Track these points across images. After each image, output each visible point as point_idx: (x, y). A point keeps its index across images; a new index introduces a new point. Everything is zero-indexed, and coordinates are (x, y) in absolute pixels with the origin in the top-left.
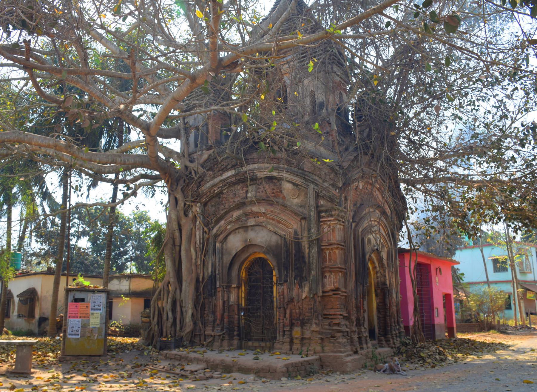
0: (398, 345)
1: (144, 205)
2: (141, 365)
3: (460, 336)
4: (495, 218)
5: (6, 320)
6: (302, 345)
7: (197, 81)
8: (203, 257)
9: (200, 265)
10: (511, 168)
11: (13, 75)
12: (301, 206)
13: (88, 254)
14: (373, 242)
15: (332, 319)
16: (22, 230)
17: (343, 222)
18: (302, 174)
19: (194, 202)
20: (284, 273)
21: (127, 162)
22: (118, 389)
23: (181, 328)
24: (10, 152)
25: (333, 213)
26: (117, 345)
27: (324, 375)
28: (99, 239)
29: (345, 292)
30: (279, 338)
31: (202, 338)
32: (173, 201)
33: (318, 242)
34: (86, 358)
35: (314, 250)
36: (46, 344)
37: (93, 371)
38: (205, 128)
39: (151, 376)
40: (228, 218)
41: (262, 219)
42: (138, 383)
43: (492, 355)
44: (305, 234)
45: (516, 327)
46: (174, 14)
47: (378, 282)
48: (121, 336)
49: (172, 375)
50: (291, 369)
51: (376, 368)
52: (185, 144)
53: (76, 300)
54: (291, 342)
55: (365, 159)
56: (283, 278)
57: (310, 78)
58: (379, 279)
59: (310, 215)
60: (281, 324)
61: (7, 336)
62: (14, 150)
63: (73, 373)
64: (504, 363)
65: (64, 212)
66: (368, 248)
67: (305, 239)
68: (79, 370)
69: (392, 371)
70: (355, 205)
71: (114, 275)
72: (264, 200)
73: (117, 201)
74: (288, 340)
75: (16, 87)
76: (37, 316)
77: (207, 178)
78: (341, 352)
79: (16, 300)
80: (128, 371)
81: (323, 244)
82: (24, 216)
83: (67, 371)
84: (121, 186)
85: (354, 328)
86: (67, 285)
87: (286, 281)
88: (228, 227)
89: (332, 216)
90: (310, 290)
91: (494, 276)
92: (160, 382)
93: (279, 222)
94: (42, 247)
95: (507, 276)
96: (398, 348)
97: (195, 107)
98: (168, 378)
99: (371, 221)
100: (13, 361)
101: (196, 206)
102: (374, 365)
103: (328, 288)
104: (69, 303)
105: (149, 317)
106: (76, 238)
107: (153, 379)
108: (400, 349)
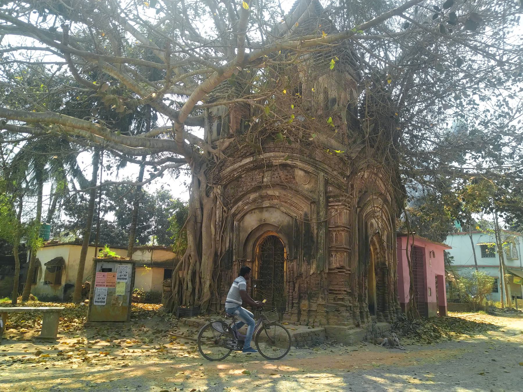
0: (395, 321)
1: (168, 185)
2: (162, 331)
3: (450, 314)
4: (487, 208)
5: (33, 287)
6: (309, 316)
7: (224, 74)
8: (221, 233)
9: (219, 241)
10: (506, 163)
11: (46, 60)
12: (311, 192)
13: (114, 227)
14: (375, 225)
15: (337, 294)
16: (51, 204)
17: (349, 207)
18: (314, 164)
19: (215, 184)
20: (294, 251)
21: (156, 146)
22: (140, 354)
23: (199, 298)
24: (44, 131)
25: (340, 198)
26: (140, 312)
27: (328, 346)
28: (124, 214)
29: (349, 271)
30: (288, 309)
31: (218, 307)
32: (196, 183)
33: (326, 225)
34: (111, 323)
35: (322, 232)
36: (71, 310)
37: (117, 336)
38: (227, 118)
39: (171, 342)
40: (245, 200)
41: (275, 201)
42: (159, 349)
43: (483, 334)
44: (315, 216)
45: (502, 309)
46: (200, 11)
47: (378, 263)
48: (142, 303)
49: (190, 341)
50: (299, 339)
51: (376, 341)
52: (209, 132)
53: (104, 270)
54: (299, 314)
55: (371, 151)
56: (293, 255)
57: (324, 76)
58: (379, 260)
59: (319, 200)
60: (290, 296)
61: (33, 302)
62: (48, 130)
63: (97, 338)
64: (497, 344)
65: (90, 187)
66: (370, 232)
67: (314, 221)
68: (103, 336)
69: (391, 345)
70: (360, 192)
71: (138, 247)
72: (278, 185)
73: (144, 180)
74: (296, 311)
75: (49, 70)
76: (63, 283)
77: (228, 163)
78: (344, 325)
79: (44, 268)
80: (149, 336)
81: (331, 226)
82: (54, 192)
83: (92, 336)
84: (148, 168)
85: (357, 304)
86: (96, 256)
87: (296, 258)
88: (245, 208)
89: (339, 201)
90: (318, 267)
91: (481, 261)
92: (179, 347)
93: (291, 205)
94: (70, 220)
95: (495, 261)
96: (395, 323)
97: (219, 98)
98: (186, 343)
99: (374, 207)
100: (39, 327)
101: (217, 188)
102: (373, 338)
103: (334, 266)
104: (97, 273)
105: (170, 286)
106: (103, 212)
107: (173, 344)
108: (397, 324)
